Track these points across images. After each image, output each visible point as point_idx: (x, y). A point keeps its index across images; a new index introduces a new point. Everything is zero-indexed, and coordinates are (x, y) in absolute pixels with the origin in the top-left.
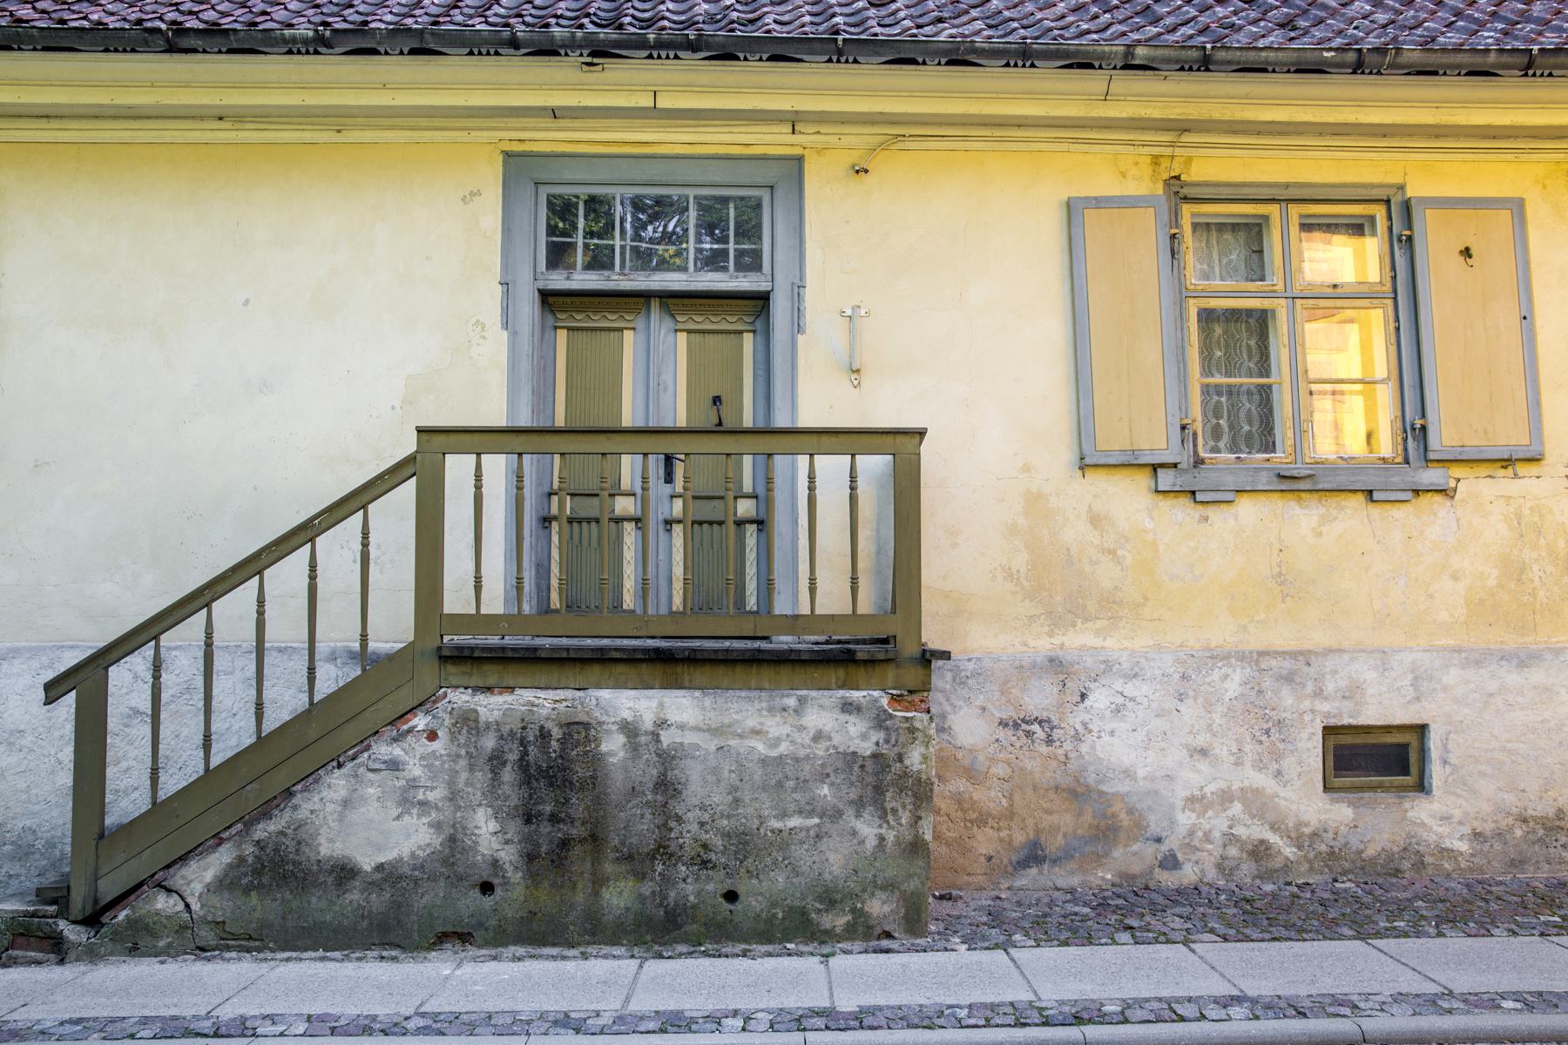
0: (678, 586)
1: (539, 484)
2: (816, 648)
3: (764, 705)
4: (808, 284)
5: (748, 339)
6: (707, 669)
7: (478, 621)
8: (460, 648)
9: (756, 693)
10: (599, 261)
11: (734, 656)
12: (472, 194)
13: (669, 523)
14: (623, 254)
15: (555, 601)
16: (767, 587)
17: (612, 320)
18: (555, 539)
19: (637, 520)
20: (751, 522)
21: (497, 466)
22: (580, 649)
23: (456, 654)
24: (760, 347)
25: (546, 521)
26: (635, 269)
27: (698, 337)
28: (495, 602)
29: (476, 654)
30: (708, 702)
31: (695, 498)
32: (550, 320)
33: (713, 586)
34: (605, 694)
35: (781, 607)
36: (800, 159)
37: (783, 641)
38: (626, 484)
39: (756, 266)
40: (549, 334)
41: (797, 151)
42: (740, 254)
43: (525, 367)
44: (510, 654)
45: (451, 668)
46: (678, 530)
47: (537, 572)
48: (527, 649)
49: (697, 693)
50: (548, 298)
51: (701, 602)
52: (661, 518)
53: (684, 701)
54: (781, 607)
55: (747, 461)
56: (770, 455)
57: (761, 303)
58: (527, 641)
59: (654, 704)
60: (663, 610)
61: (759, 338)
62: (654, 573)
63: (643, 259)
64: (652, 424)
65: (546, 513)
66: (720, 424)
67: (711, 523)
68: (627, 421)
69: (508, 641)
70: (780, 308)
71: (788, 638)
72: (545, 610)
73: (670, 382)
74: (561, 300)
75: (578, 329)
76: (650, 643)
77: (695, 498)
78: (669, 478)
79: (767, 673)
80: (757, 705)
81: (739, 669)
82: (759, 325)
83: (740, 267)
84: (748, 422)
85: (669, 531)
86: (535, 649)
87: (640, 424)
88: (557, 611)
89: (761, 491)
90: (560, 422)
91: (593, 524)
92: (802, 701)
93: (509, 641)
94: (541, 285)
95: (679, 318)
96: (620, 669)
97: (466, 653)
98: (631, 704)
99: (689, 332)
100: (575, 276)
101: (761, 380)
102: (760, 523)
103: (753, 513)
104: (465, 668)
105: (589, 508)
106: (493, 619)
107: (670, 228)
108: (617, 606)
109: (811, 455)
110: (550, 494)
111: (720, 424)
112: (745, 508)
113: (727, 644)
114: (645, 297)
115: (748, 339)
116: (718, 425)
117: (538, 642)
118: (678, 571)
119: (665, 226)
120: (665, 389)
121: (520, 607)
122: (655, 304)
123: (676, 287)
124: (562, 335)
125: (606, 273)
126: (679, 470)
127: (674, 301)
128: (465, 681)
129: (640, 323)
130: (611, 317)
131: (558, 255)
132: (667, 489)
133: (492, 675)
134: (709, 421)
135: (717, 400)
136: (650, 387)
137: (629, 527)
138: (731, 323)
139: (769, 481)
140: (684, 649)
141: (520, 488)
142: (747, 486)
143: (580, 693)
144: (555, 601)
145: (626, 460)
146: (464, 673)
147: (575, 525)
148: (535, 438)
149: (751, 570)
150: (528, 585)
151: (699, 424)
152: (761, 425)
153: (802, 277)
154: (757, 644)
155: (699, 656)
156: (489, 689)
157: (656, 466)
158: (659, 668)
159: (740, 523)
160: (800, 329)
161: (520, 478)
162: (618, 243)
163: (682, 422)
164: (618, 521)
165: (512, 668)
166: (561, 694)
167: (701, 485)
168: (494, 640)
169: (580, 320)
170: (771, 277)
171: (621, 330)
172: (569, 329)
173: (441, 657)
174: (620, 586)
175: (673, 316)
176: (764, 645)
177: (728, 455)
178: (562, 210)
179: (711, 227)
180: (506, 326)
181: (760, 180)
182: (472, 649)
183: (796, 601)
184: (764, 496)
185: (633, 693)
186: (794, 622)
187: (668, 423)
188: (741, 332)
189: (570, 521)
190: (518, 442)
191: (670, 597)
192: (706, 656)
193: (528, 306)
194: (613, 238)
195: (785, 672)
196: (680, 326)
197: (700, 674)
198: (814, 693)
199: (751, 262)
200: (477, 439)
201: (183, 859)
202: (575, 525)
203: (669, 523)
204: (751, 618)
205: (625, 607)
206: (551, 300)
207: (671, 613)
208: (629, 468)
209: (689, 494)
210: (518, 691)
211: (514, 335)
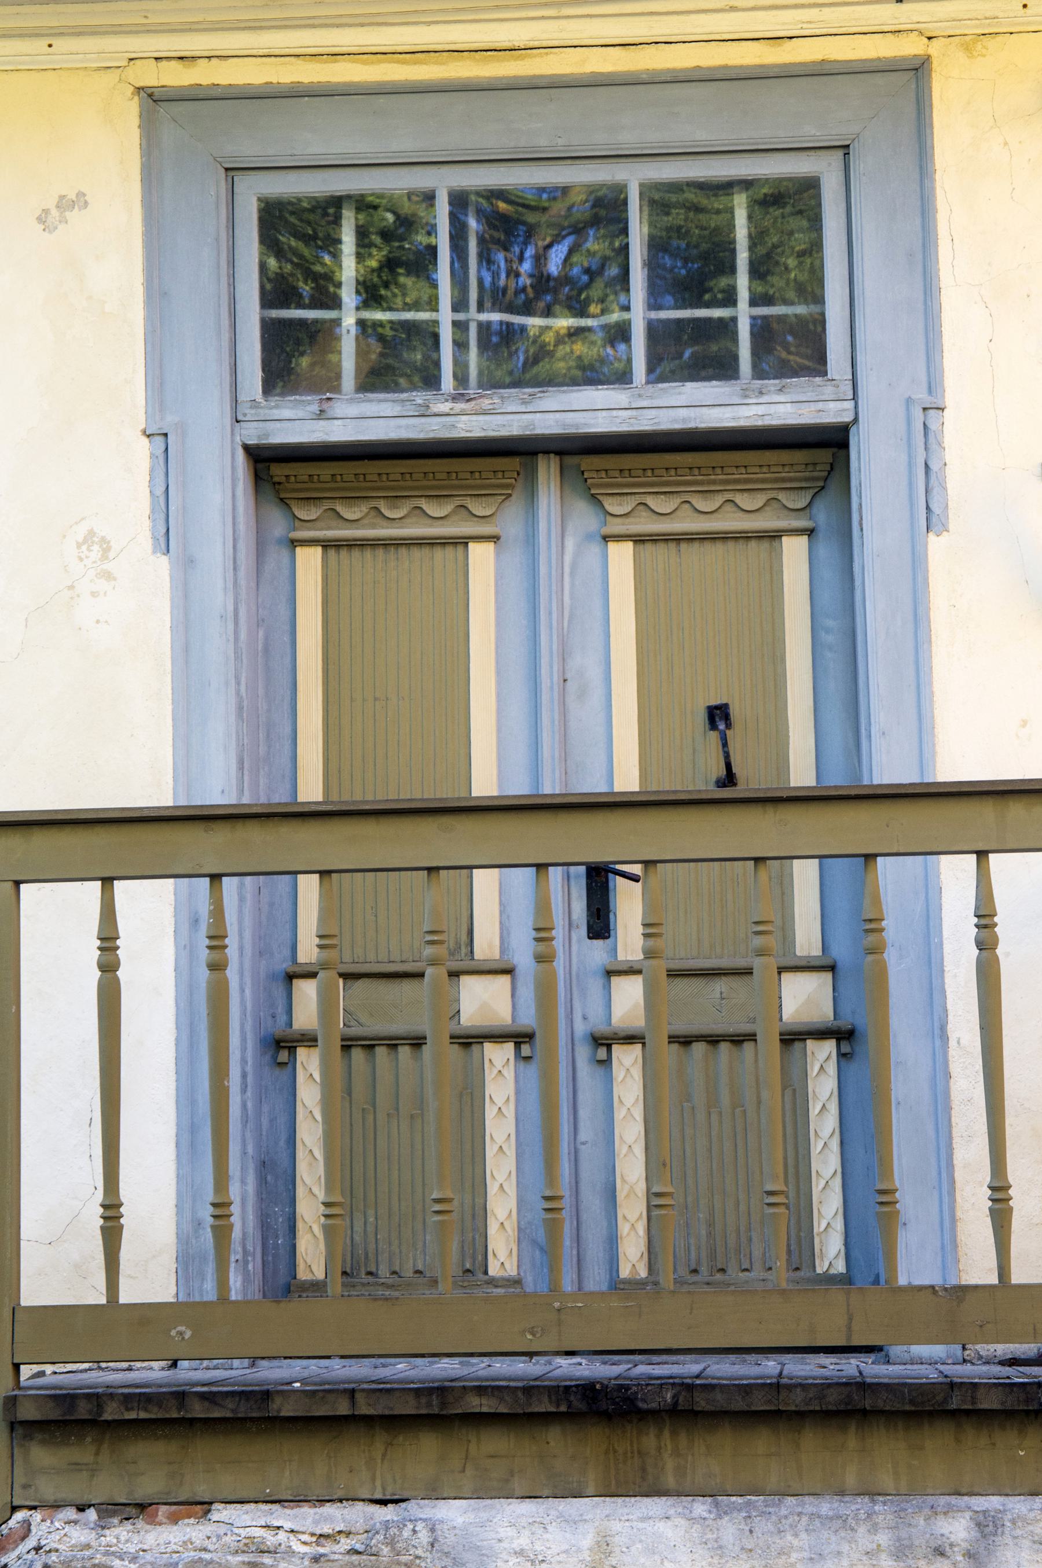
0: (632, 1214)
1: (262, 952)
2: (1018, 1375)
3: (883, 1538)
4: (950, 399)
5: (794, 551)
6: (725, 1439)
7: (111, 1323)
8: (65, 1399)
9: (862, 1503)
10: (398, 361)
11: (796, 1401)
12: (65, 204)
13: (604, 1042)
14: (460, 345)
15: (312, 1257)
16: (874, 1210)
17: (438, 518)
18: (309, 1095)
19: (520, 1038)
20: (821, 1034)
21: (151, 909)
22: (383, 1390)
23: (54, 1414)
24: (829, 575)
25: (282, 1047)
26: (490, 383)
27: (660, 553)
28: (151, 1277)
29: (110, 1414)
30: (729, 1529)
31: (674, 974)
32: (278, 524)
33: (726, 1203)
34: (454, 1514)
35: (915, 1266)
36: (918, 70)
37: (923, 1358)
38: (486, 943)
39: (815, 362)
40: (277, 556)
41: (910, 47)
42: (765, 334)
43: (217, 646)
44: (198, 1410)
45: (41, 1455)
46: (627, 1060)
47: (262, 1181)
48: (244, 1395)
49: (701, 1507)
50: (276, 471)
51: (700, 1251)
52: (580, 1028)
53: (662, 1527)
54: (915, 1266)
55: (805, 876)
56: (869, 858)
57: (824, 456)
58: (235, 1372)
59: (587, 1540)
60: (596, 1280)
61: (825, 550)
62: (565, 1182)
63: (514, 362)
64: (551, 787)
65: (279, 1028)
66: (729, 779)
67: (713, 1040)
68: (485, 783)
69: (189, 1373)
70: (874, 461)
71: (937, 1350)
72: (284, 1285)
73: (594, 674)
74: (303, 470)
75: (351, 544)
76: (566, 1368)
77: (674, 974)
78: (600, 924)
79: (888, 1449)
80: (864, 1539)
81: (810, 1439)
82: (822, 515)
83: (377, 378)
84: (802, 774)
85: (606, 1063)
86: (265, 1395)
87: (519, 787)
88: (316, 1287)
89: (841, 952)
90: (311, 790)
91: (404, 1051)
92: (987, 1527)
93: (191, 1373)
94: (252, 434)
95: (612, 506)
96: (493, 1443)
97: (83, 1411)
98: (523, 1541)
99: (639, 540)
100: (341, 408)
101: (834, 662)
102: (844, 1036)
103: (824, 1012)
104: (81, 1453)
105: (398, 1009)
106: (147, 1315)
107: (554, 265)
108: (474, 1268)
109: (982, 855)
110: (290, 977)
111: (729, 779)
112: (803, 998)
113: (770, 1366)
114: (519, 454)
115: (794, 551)
116: (723, 781)
117: (271, 1372)
118: (632, 1171)
119: (540, 259)
120: (583, 694)
121: (222, 1284)
122: (547, 471)
123: (601, 424)
124: (310, 561)
125: (419, 397)
126: (629, 904)
127: (588, 457)
128: (75, 1488)
129: (510, 520)
130: (433, 509)
131: (290, 354)
132: (597, 952)
133: (149, 1467)
134: (701, 773)
135: (718, 716)
136: (545, 685)
137: (499, 1057)
138: (747, 511)
139: (871, 925)
140: (663, 1383)
141: (217, 967)
142: (807, 939)
143: (388, 1513)
144: (312, 1257)
145: (486, 884)
146: (76, 1467)
147: (357, 1054)
148: (253, 832)
149: (826, 1163)
150: (243, 1220)
151: (668, 784)
152: (837, 779)
153: (934, 383)
154: (850, 1366)
155: (701, 1403)
156: (140, 1509)
157: (569, 900)
158: (594, 1441)
159: (793, 1038)
160: (932, 520)
161: (217, 940)
162: (445, 317)
163: (628, 780)
164: (469, 1041)
165: (205, 1448)
166: (336, 1516)
167: (685, 947)
168: (152, 1372)
169: (357, 521)
170: (857, 387)
171: (462, 542)
172: (327, 545)
173: (12, 1426)
174: (479, 1215)
175: (595, 500)
176: (872, 1369)
177: (758, 860)
178: (294, 233)
179: (693, 265)
180: (164, 542)
181: (811, 132)
182: (97, 1398)
183: (949, 1246)
184: (855, 960)
185: (527, 1507)
186: (954, 1306)
187: (591, 783)
188: (774, 536)
189: (348, 1045)
190: (210, 846)
191: (612, 1241)
192: (720, 1401)
193: (220, 487)
194: (730, 299)
195: (936, 1442)
196: (616, 527)
197: (710, 1454)
198: (1018, 1505)
199: (796, 348)
200: (101, 840)
201: (263, 1358)
202: (357, 1054)
203: (604, 1042)
204: (837, 1295)
205: (494, 1270)
206: (278, 471)
207: (618, 1286)
208: (495, 904)
209: (661, 966)
210: (221, 1513)
211: (186, 567)
